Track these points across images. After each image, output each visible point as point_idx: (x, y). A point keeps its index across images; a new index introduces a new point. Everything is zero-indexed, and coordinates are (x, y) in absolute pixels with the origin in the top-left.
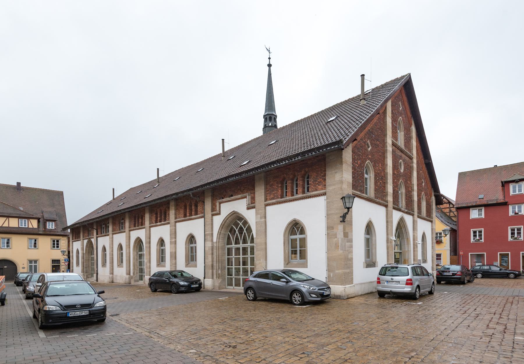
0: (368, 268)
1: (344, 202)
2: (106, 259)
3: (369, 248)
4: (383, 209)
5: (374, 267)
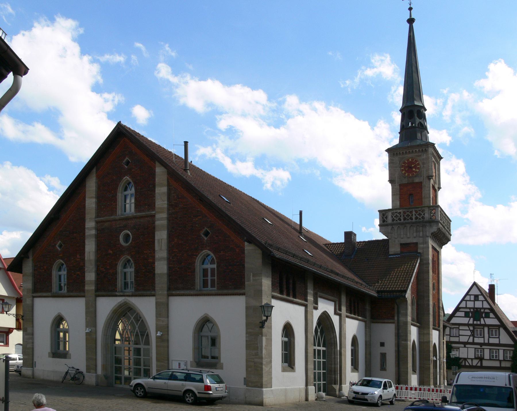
4: (303, 308)
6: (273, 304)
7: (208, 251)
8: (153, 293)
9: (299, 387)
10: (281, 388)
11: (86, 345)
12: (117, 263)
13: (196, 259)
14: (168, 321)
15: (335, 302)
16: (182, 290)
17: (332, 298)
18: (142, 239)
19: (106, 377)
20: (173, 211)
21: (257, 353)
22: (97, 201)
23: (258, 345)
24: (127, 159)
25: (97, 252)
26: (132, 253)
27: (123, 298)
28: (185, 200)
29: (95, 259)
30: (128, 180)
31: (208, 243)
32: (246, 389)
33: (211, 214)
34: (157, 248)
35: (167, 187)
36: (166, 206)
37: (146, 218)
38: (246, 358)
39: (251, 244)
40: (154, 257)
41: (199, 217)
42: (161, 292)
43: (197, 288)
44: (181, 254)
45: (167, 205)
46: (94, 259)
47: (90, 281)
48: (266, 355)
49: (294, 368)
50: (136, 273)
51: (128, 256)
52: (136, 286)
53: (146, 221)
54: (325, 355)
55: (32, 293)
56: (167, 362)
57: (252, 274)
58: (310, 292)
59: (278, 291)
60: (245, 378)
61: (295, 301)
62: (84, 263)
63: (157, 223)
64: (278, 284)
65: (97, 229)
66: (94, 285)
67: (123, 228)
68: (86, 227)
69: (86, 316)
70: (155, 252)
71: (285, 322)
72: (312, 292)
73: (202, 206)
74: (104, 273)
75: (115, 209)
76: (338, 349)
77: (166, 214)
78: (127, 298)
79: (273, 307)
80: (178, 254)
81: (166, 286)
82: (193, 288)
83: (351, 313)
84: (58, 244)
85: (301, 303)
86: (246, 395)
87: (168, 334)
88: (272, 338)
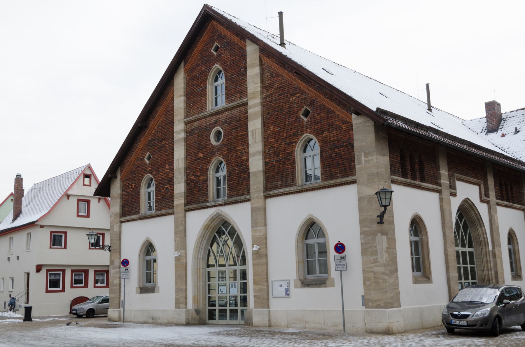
0: (143, 293)
1: (379, 198)
2: (511, 257)
3: (419, 255)
4: (436, 195)
5: (153, 293)
6: (392, 190)
7: (309, 135)
8: (248, 197)
9: (439, 304)
10: (413, 307)
11: (175, 273)
12: (207, 167)
13: (295, 147)
14: (266, 230)
15: (479, 185)
16: (281, 188)
17: (475, 180)
18: (234, 134)
19: (197, 311)
20: (267, 94)
21: (377, 259)
22: (185, 98)
23: (378, 248)
24: (217, 45)
25: (187, 158)
26: (224, 153)
27: (215, 208)
28: (280, 78)
29: (184, 167)
30: (218, 69)
31: (309, 124)
32: (366, 311)
33: (310, 89)
34: (250, 141)
35: (259, 67)
36: (260, 89)
37: (238, 109)
38: (363, 268)
39: (359, 116)
40: (247, 153)
41: (297, 95)
42: (256, 195)
43: (298, 183)
44: (278, 144)
45: (260, 88)
46: (183, 166)
47: (179, 193)
48: (389, 261)
49: (430, 277)
50: (229, 177)
51: (220, 157)
52: (229, 192)
53: (238, 112)
54: (473, 259)
55: (120, 218)
56: (266, 283)
57: (363, 153)
58: (444, 172)
59: (399, 174)
60: (363, 296)
61: (424, 186)
62: (173, 174)
63: (250, 111)
64: (398, 165)
65: (186, 131)
66: (184, 198)
67: (213, 125)
68: (175, 130)
69: (176, 237)
70: (248, 147)
71: (412, 215)
72: (446, 173)
73: (299, 81)
74: (195, 182)
75: (205, 104)
76: (490, 248)
77: (259, 99)
78: (219, 208)
79: (392, 193)
80: (274, 144)
81: (263, 186)
82: (293, 183)
83: (502, 199)
84: (146, 157)
85: (432, 188)
86: (366, 319)
87: (266, 247)
88: (395, 237)
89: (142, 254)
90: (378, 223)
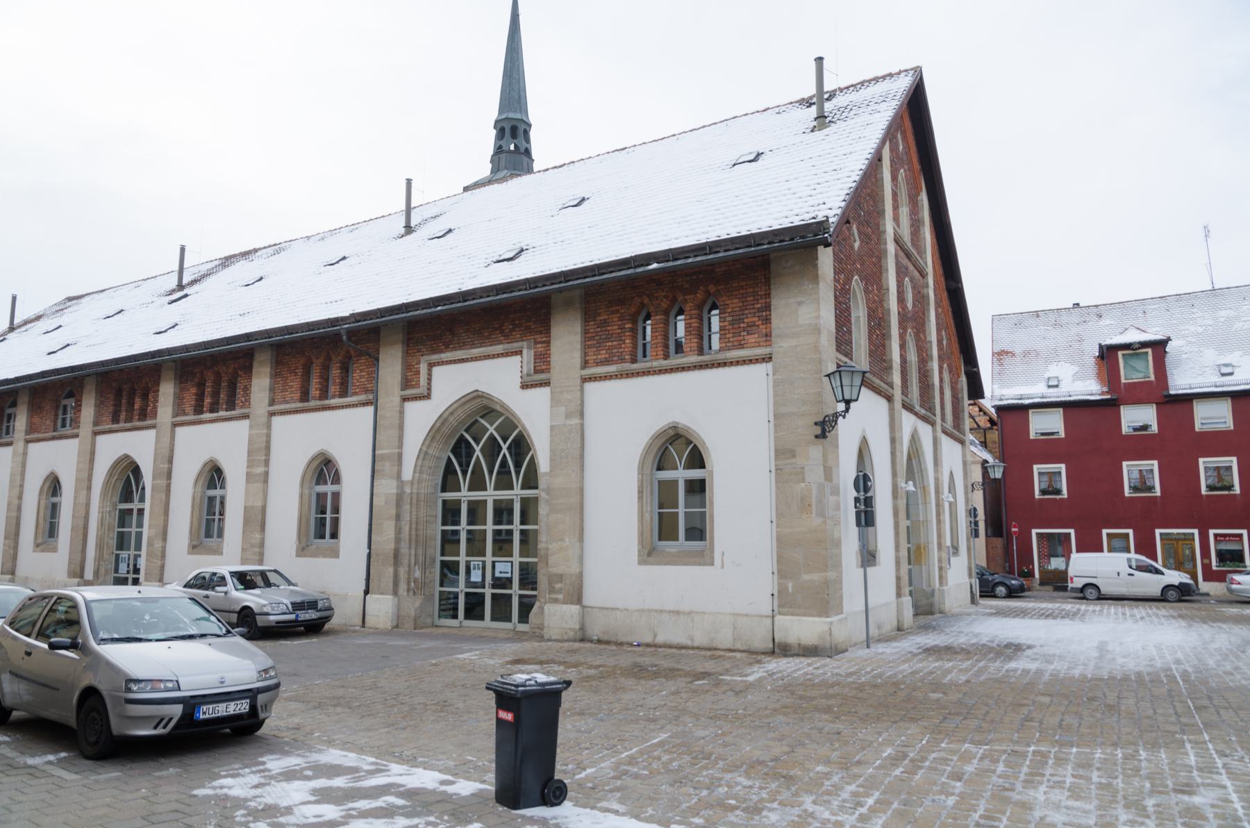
89: (200, 483)
90: (817, 437)
